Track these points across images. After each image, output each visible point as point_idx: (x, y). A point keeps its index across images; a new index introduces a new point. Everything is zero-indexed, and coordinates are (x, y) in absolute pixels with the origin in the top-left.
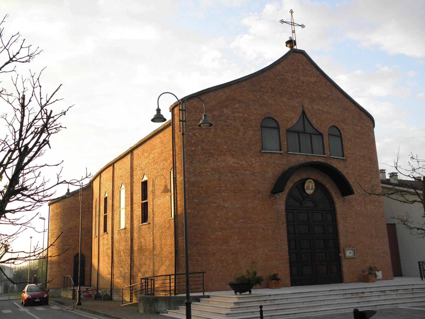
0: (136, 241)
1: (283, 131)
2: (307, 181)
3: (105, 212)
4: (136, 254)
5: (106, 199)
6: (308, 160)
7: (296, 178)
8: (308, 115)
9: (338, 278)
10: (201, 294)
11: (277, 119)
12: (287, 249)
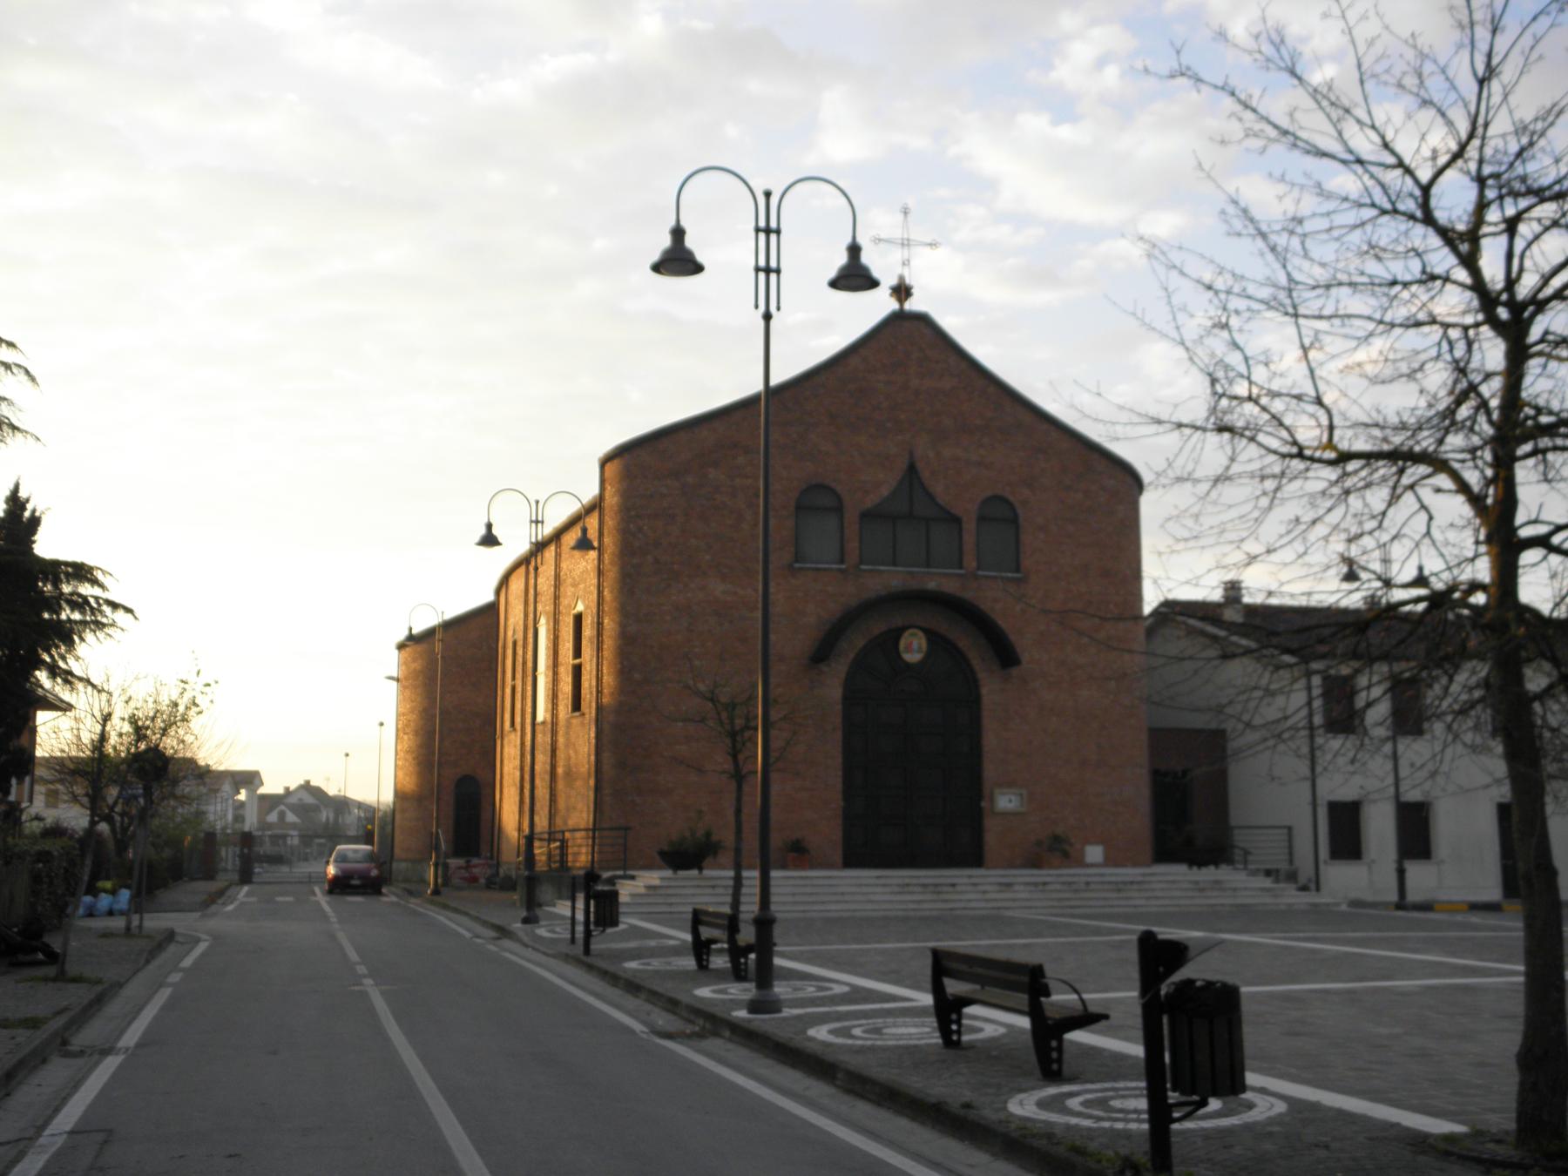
0: (561, 755)
1: (851, 516)
2: (906, 634)
3: (578, 653)
4: (561, 785)
5: (578, 619)
6: (914, 585)
7: (878, 627)
8: (925, 475)
9: (972, 856)
10: (620, 873)
11: (838, 489)
12: (840, 786)
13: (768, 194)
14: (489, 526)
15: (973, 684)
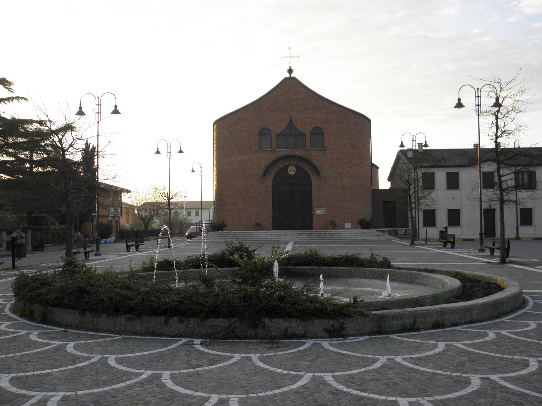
6: (292, 153)
7: (281, 165)
11: (270, 128)
13: (478, 89)
14: (181, 148)
15: (310, 180)
